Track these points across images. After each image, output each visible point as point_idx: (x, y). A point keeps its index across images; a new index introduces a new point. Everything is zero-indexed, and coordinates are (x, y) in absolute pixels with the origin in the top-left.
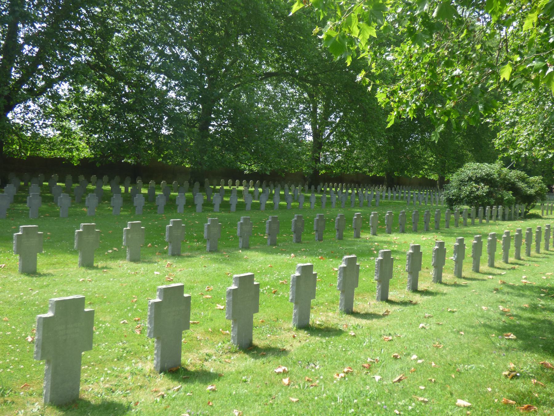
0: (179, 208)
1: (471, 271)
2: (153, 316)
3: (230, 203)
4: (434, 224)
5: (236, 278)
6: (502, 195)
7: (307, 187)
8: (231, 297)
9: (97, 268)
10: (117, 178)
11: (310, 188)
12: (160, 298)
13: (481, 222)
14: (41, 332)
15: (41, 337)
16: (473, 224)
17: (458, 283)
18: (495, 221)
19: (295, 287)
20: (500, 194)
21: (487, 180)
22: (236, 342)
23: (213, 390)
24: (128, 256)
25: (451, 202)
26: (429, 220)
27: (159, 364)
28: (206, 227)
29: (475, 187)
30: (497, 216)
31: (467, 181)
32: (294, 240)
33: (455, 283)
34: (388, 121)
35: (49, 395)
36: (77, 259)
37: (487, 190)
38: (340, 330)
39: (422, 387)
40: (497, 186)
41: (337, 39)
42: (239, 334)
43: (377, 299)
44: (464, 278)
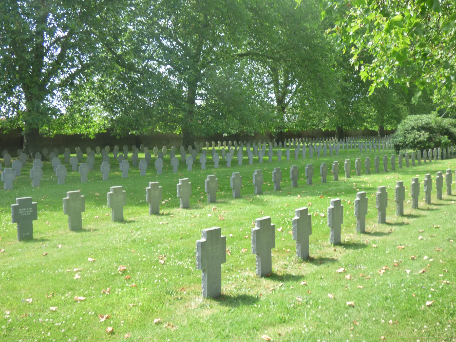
0: (188, 167)
1: (436, 198)
2: (255, 239)
3: (226, 160)
4: (391, 166)
5: (298, 211)
6: (439, 139)
7: (276, 143)
8: (296, 225)
9: (163, 215)
10: (125, 148)
11: (278, 144)
12: (258, 226)
13: (425, 162)
14: (200, 252)
15: (200, 255)
16: (420, 164)
17: (430, 208)
18: (436, 160)
19: (331, 216)
20: (438, 138)
21: (426, 128)
22: (300, 255)
23: (305, 285)
24: (181, 205)
25: (397, 148)
26: (387, 163)
27: (260, 272)
28: (231, 179)
29: (418, 134)
30: (437, 156)
31: (411, 130)
32: (292, 185)
33: (428, 208)
34: (369, 90)
35: (206, 292)
36: (148, 209)
37: (428, 136)
38: (364, 244)
39: (442, 275)
40: (435, 133)
41: (400, 53)
42: (302, 250)
43: (379, 223)
44: (433, 204)
